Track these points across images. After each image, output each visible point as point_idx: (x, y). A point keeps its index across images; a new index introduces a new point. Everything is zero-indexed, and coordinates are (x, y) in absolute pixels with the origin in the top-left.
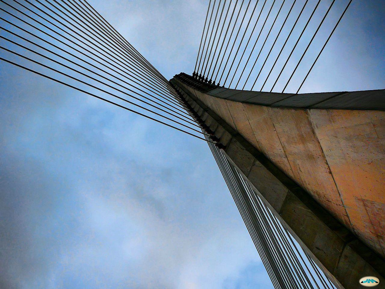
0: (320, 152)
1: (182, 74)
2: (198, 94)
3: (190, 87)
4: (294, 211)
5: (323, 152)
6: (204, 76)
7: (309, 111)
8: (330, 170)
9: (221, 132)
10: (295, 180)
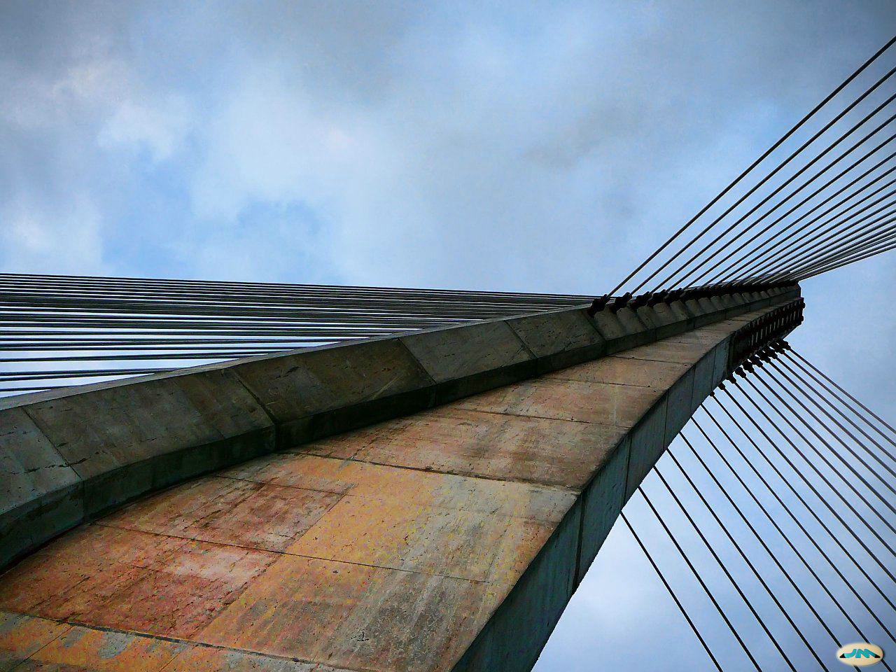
0: (479, 472)
1: (799, 320)
2: (738, 323)
3: (756, 320)
4: (389, 370)
5: (476, 476)
6: (768, 361)
7: (576, 493)
8: (434, 471)
9: (628, 323)
10: (450, 407)
